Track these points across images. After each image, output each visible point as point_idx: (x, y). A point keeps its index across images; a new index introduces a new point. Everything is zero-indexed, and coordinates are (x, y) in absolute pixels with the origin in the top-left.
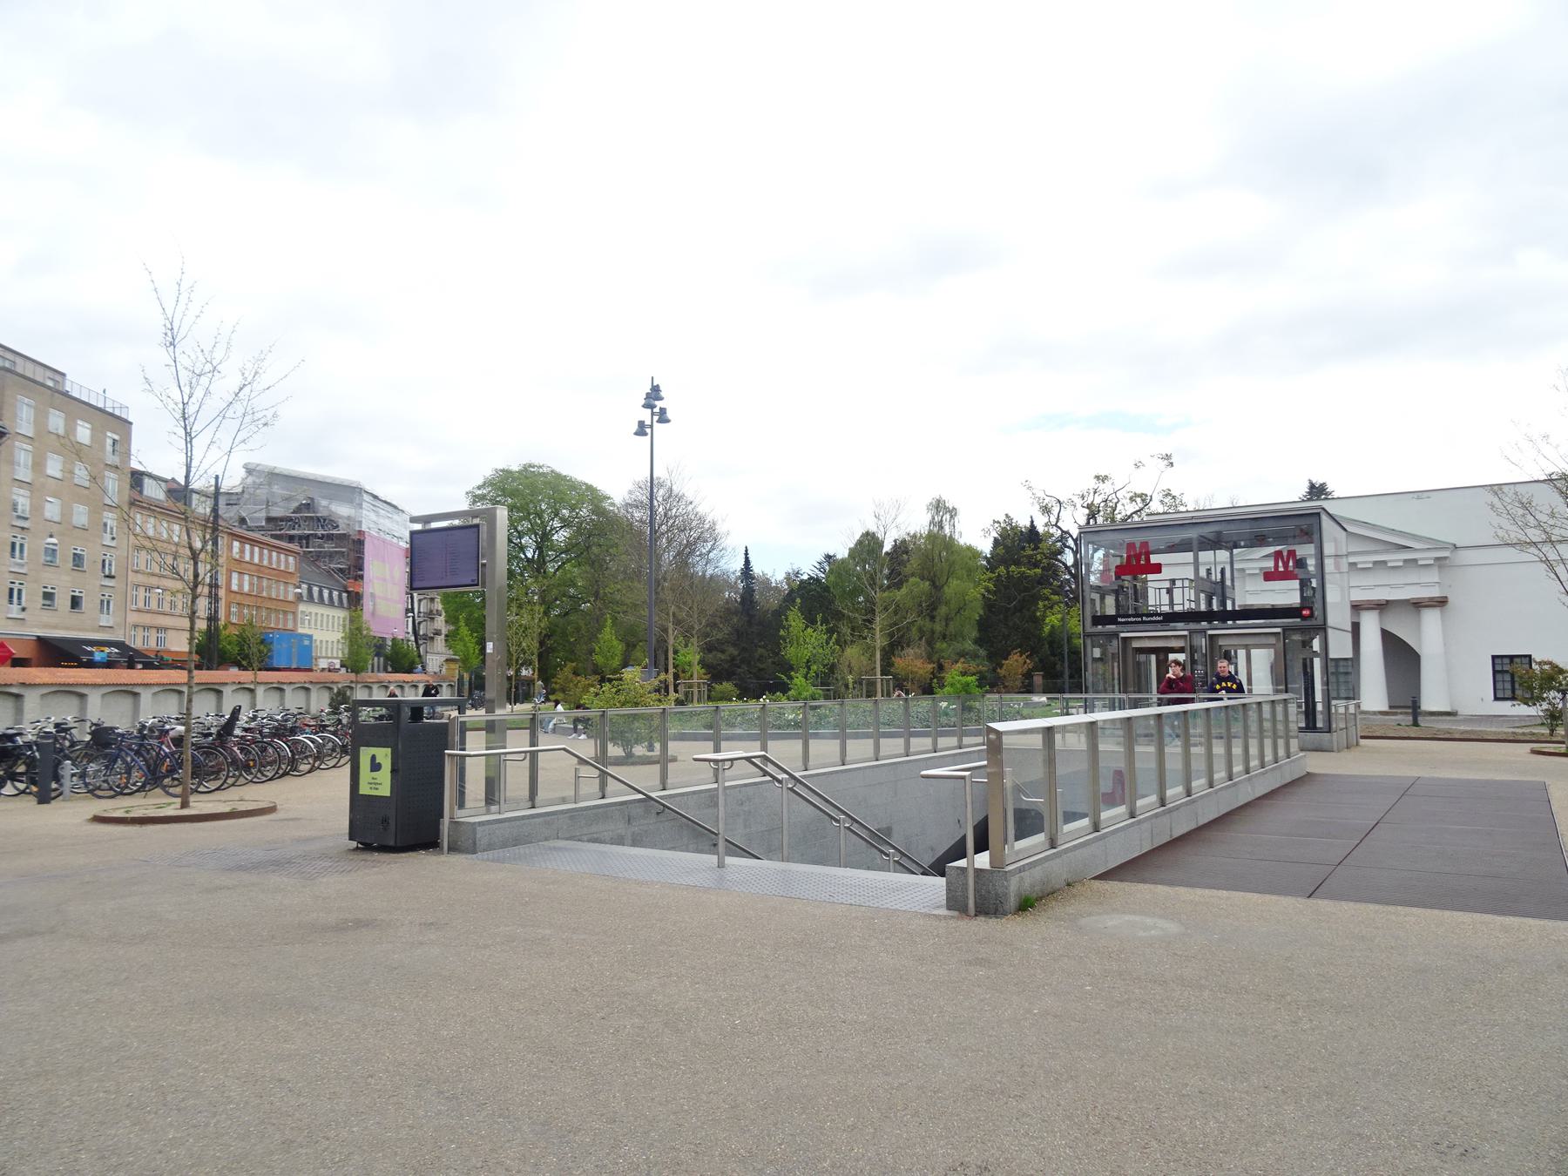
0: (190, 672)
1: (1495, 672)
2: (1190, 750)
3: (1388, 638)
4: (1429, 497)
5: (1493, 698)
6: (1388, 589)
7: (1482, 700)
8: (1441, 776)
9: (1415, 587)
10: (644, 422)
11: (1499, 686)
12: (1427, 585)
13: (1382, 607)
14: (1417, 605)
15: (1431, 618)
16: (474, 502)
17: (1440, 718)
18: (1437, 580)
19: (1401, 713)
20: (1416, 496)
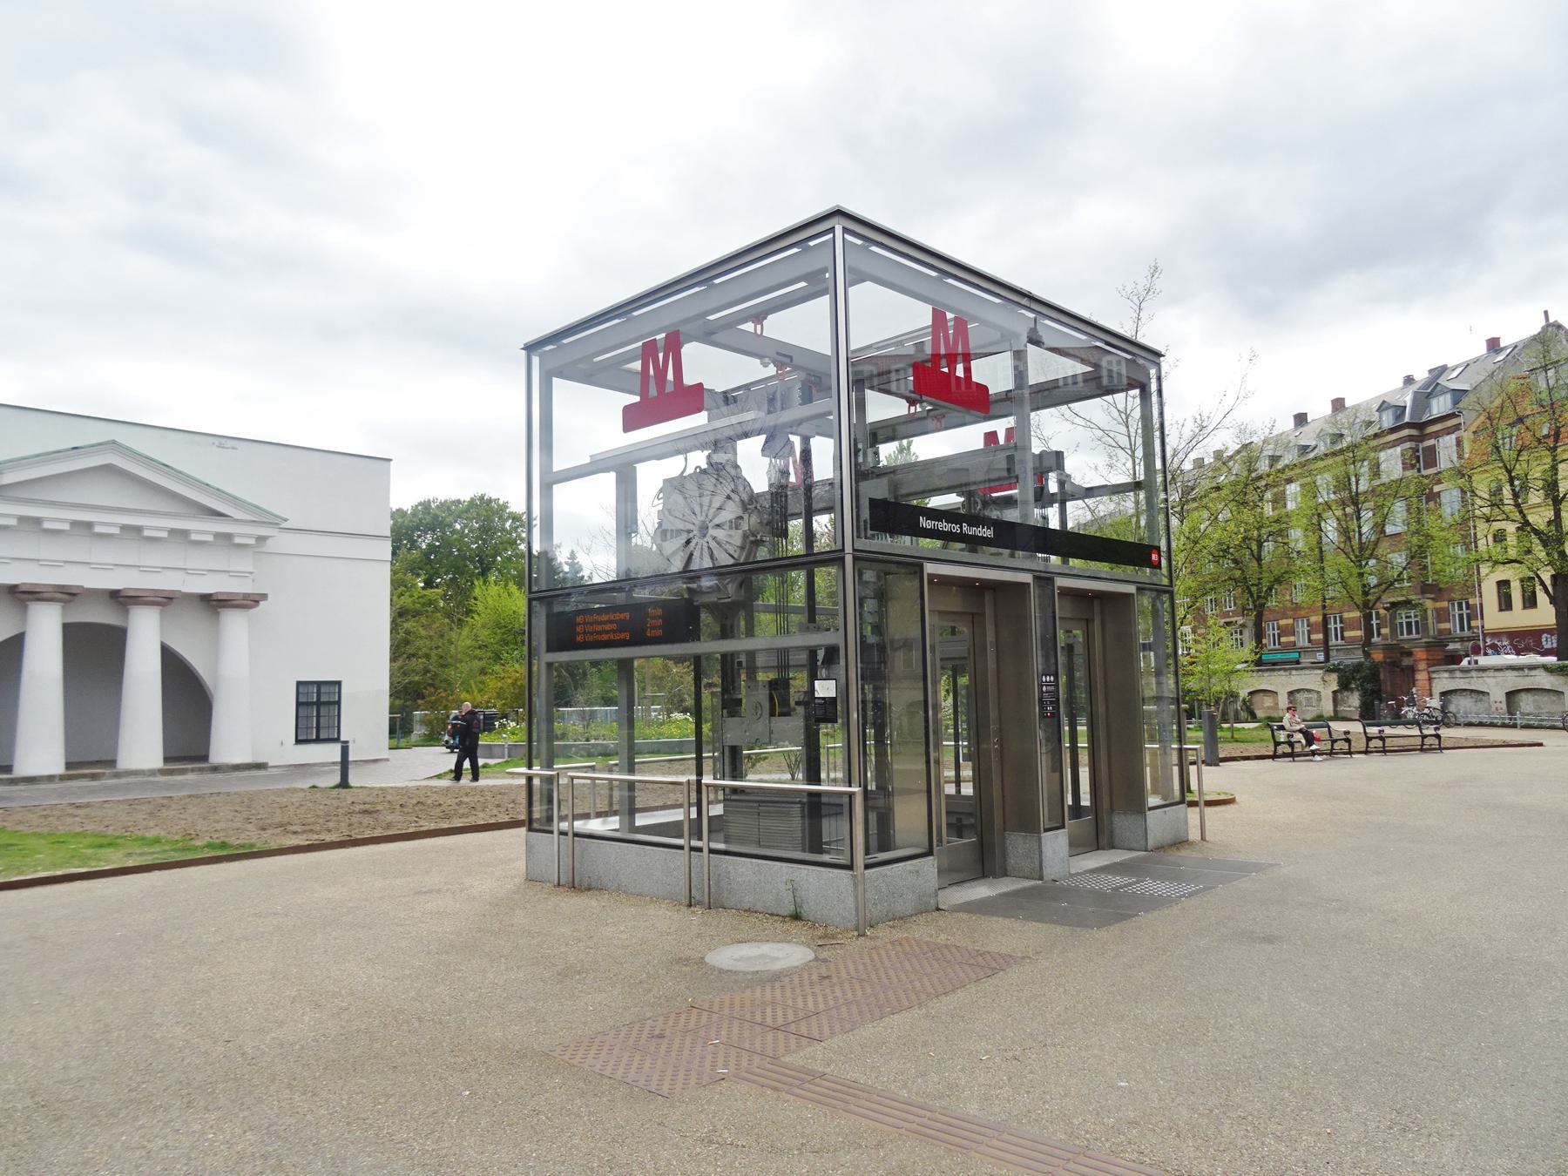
0: (399, 739)
1: (299, 704)
2: (974, 788)
3: (168, 656)
4: (234, 448)
5: (294, 742)
6: (181, 574)
7: (282, 743)
8: (38, 876)
9: (222, 575)
10: (1343, 399)
11: (302, 723)
12: (241, 575)
13: (165, 601)
14: (213, 604)
15: (235, 624)
16: (1333, 443)
17: (246, 773)
18: (250, 569)
19: (192, 770)
20: (217, 443)
